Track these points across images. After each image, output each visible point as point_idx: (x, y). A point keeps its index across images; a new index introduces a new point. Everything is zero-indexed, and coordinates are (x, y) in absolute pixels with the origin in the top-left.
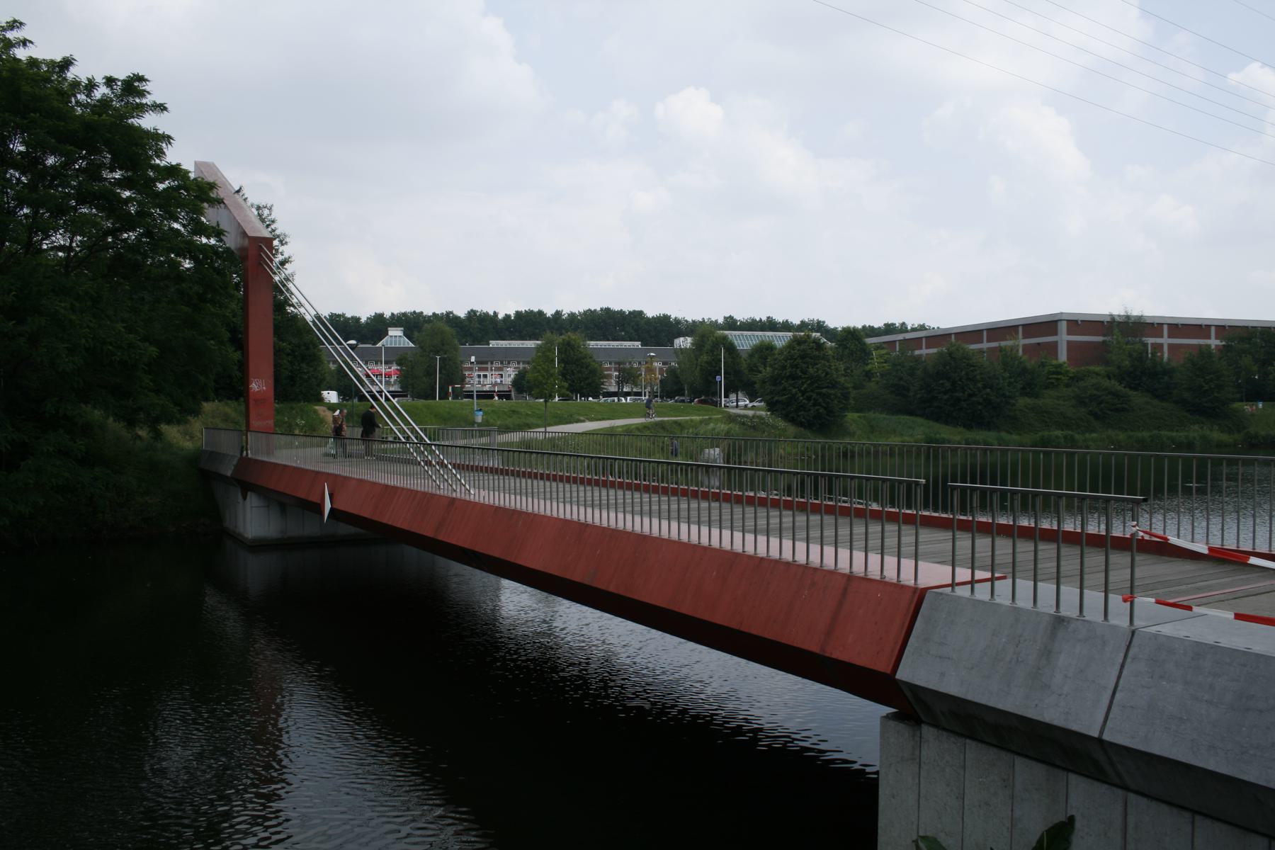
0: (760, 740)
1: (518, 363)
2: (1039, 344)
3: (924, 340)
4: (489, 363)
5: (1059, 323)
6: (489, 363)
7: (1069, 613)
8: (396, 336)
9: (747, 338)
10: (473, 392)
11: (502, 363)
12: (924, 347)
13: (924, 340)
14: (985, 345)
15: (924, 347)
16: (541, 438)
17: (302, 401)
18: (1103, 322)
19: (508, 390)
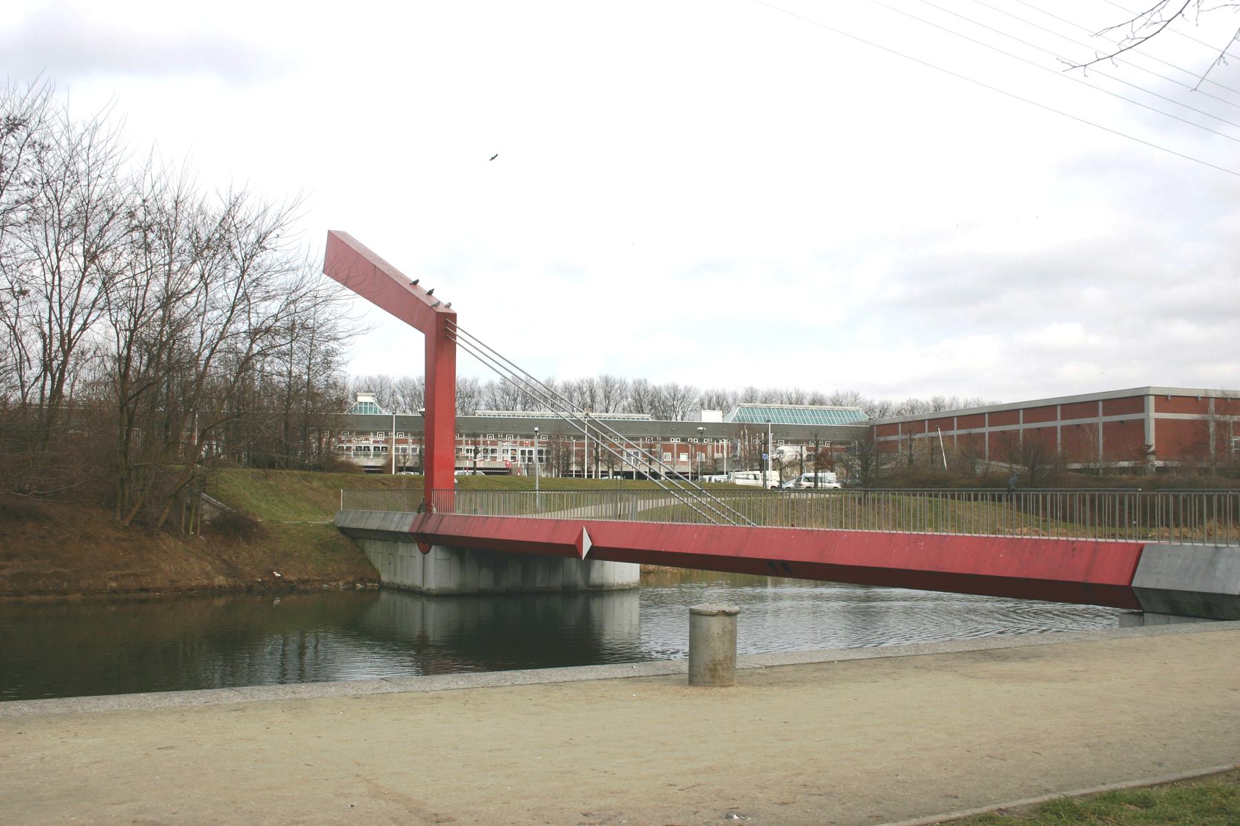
0: (9, 708)
1: (515, 437)
2: (1122, 422)
3: (987, 415)
4: (641, 440)
5: (1146, 398)
6: (641, 440)
7: (988, 605)
8: (366, 403)
9: (801, 413)
10: (688, 473)
11: (496, 436)
12: (1059, 430)
13: (987, 415)
14: (1021, 426)
15: (1059, 430)
16: (672, 504)
17: (312, 471)
18: (1196, 398)
19: (505, 467)
